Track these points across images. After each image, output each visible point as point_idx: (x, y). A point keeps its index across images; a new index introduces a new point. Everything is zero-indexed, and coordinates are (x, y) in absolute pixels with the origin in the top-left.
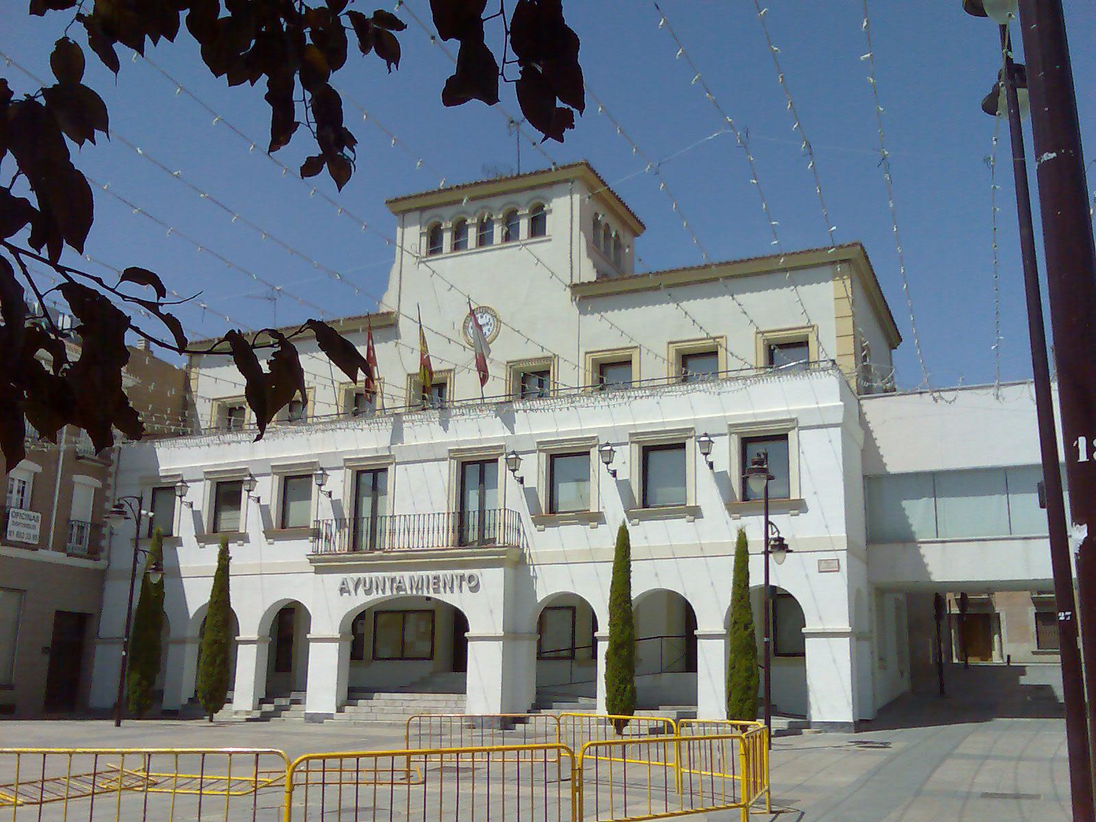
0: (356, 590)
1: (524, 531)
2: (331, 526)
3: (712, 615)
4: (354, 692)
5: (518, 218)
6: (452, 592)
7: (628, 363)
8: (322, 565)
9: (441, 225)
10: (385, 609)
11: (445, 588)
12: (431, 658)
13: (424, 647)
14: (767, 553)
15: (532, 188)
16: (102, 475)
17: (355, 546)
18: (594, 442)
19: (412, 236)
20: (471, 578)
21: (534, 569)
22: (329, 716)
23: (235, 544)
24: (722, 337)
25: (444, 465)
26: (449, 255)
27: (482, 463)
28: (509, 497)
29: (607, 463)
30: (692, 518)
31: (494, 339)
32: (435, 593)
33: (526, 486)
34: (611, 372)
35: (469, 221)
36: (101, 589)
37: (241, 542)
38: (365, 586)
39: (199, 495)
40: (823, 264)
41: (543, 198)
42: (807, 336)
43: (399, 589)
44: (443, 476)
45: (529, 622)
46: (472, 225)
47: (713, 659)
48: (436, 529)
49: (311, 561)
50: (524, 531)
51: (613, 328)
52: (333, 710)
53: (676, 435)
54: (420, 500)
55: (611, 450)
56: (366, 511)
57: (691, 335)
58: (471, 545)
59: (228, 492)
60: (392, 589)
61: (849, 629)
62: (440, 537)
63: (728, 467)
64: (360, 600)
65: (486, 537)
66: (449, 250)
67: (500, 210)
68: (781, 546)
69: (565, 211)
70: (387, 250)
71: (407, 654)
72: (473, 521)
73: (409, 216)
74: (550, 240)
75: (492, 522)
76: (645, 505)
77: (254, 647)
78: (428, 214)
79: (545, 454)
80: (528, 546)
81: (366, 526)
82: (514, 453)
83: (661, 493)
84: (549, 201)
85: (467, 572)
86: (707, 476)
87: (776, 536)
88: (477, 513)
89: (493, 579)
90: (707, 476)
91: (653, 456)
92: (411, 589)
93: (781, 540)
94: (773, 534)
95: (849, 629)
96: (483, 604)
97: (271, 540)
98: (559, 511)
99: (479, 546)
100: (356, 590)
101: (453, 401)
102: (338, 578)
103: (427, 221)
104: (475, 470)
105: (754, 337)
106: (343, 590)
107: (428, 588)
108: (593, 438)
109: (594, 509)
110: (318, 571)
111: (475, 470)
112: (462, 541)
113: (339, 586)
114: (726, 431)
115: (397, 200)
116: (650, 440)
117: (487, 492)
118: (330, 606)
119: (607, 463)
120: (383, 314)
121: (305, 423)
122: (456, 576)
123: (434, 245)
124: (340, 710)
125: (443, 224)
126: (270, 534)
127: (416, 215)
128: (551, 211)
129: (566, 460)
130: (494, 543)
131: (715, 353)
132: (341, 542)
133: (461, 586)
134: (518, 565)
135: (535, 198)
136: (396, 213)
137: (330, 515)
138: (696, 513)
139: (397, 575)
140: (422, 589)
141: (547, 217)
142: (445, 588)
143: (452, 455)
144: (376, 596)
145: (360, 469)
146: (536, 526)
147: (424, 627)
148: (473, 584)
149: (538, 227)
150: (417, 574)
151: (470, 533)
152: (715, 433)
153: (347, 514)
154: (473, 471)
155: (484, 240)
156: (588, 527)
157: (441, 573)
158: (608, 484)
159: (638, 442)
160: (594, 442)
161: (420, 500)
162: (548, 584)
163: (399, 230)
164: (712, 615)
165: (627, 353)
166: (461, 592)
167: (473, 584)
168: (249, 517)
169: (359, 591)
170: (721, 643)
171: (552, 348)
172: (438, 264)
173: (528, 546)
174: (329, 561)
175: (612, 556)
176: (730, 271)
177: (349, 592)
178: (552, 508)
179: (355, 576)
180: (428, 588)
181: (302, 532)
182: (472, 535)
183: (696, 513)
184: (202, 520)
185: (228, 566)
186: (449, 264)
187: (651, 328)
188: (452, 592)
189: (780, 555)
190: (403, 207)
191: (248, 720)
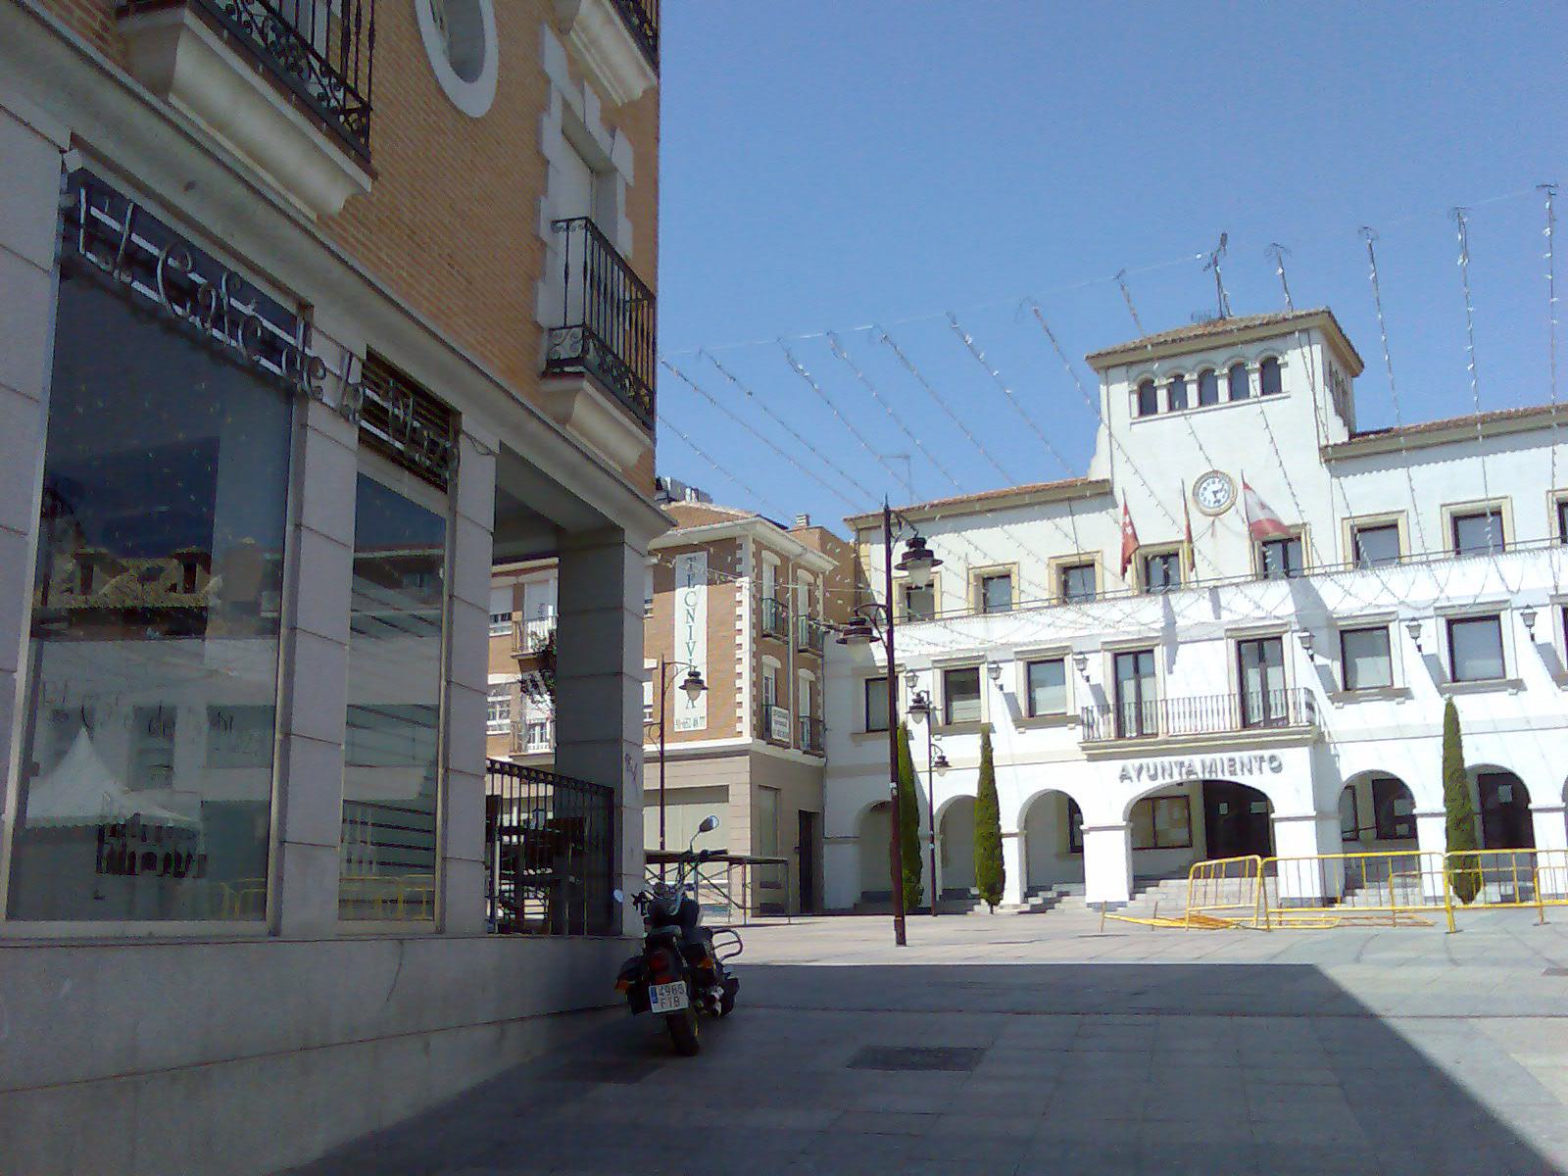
0: (1138, 777)
1: (1319, 709)
2: (1092, 711)
3: (1428, 794)
4: (1140, 881)
5: (1247, 373)
6: (1251, 774)
7: (1007, 576)
8: (1095, 753)
9: (1153, 382)
10: (1166, 794)
11: (1242, 770)
12: (1190, 845)
13: (1180, 835)
14: (930, 772)
15: (1261, 339)
16: (813, 667)
17: (1120, 733)
18: (1393, 617)
19: (1120, 396)
20: (1272, 758)
21: (1335, 748)
22: (1122, 904)
23: (1066, 728)
24: (1506, 498)
25: (1221, 644)
26: (1165, 415)
27: (1136, 655)
28: (1301, 670)
29: (995, 679)
30: (1515, 691)
31: (1227, 510)
32: (1231, 775)
33: (1425, 654)
34: (1375, 541)
35: (1187, 378)
36: (822, 787)
37: (1073, 725)
38: (1149, 771)
39: (931, 684)
40: (1062, 500)
41: (1274, 350)
42: (1397, 520)
43: (1189, 773)
44: (1222, 656)
45: (1332, 802)
46: (1192, 381)
47: (1432, 836)
48: (1182, 715)
49: (1084, 749)
50: (1319, 709)
51: (1376, 491)
52: (1126, 898)
53: (1490, 607)
54: (1197, 683)
55: (998, 667)
56: (1129, 695)
57: (1067, 550)
58: (1256, 726)
59: (962, 682)
60: (1181, 774)
61: (1314, 814)
62: (1226, 720)
63: (1553, 636)
64: (1144, 786)
65: (1273, 717)
66: (1227, 398)
67: (1193, 370)
68: (943, 763)
69: (1303, 365)
70: (1093, 415)
71: (1160, 844)
72: (1255, 702)
73: (1112, 372)
74: (1289, 397)
75: (1148, 711)
76: (1455, 679)
77: (1016, 839)
78: (1135, 370)
79: (1233, 640)
80: (1325, 724)
81: (1130, 712)
82: (911, 671)
83: (1471, 666)
84: (1282, 353)
85: (1267, 753)
86: (1412, 659)
87: (939, 754)
88: (1260, 695)
89: (1297, 761)
90: (1412, 659)
91: (1346, 635)
92: (1203, 773)
93: (943, 758)
94: (936, 753)
95: (1314, 814)
96: (1288, 787)
97: (1022, 730)
98: (1359, 686)
99: (1265, 727)
100: (1138, 777)
101: (1105, 593)
102: (1116, 765)
103: (1137, 377)
104: (1256, 650)
105: (1545, 498)
106: (1124, 777)
107: (1223, 771)
108: (1393, 613)
109: (1398, 684)
110: (1092, 758)
111: (1256, 650)
112: (1246, 723)
113: (1118, 773)
114: (1548, 602)
115: (1100, 355)
116: (1452, 613)
117: (1143, 681)
118: (1106, 796)
119: (1082, 670)
120: (1097, 482)
121: (1400, 564)
122: (1176, 764)
123: (1147, 407)
124: (1132, 898)
125: (1280, 358)
126: (1019, 723)
127: (1124, 369)
128: (1286, 364)
129: (1043, 666)
130: (1287, 725)
131: (1093, 565)
132: (1105, 728)
133: (1261, 769)
134: (1318, 742)
135: (1233, 357)
136: (1097, 370)
137: (1090, 702)
138: (1518, 685)
139: (1186, 759)
140: (1216, 772)
141: (1282, 370)
142: (1242, 770)
143: (1229, 634)
144: (1160, 782)
145: (1030, 660)
146: (1333, 703)
147: (1178, 813)
148: (1275, 764)
149: (1271, 384)
150: (1208, 758)
151: (1257, 716)
152: (1537, 604)
153: (1111, 701)
154: (1127, 663)
155: (1177, 401)
156: (1394, 703)
157: (1236, 755)
158: (1084, 689)
159: (1560, 604)
160: (1393, 617)
161: (1197, 683)
162: (1352, 763)
163: (1103, 388)
164: (1428, 794)
165: (1394, 517)
166: (1261, 773)
167: (1275, 764)
168: (992, 705)
169: (1141, 777)
170: (1121, 834)
171: (1088, 546)
172: (1151, 426)
173: (1325, 724)
174: (1106, 747)
175: (1441, 731)
176: (987, 505)
177: (1130, 778)
178: (1032, 712)
179: (1137, 762)
180: (1223, 771)
181: (1061, 720)
182: (1256, 717)
183: (1518, 685)
184: (1440, 664)
185: (991, 758)
186: (1166, 426)
187: (1421, 492)
188: (1251, 774)
189: (942, 770)
190: (1107, 363)
191: (1021, 913)
